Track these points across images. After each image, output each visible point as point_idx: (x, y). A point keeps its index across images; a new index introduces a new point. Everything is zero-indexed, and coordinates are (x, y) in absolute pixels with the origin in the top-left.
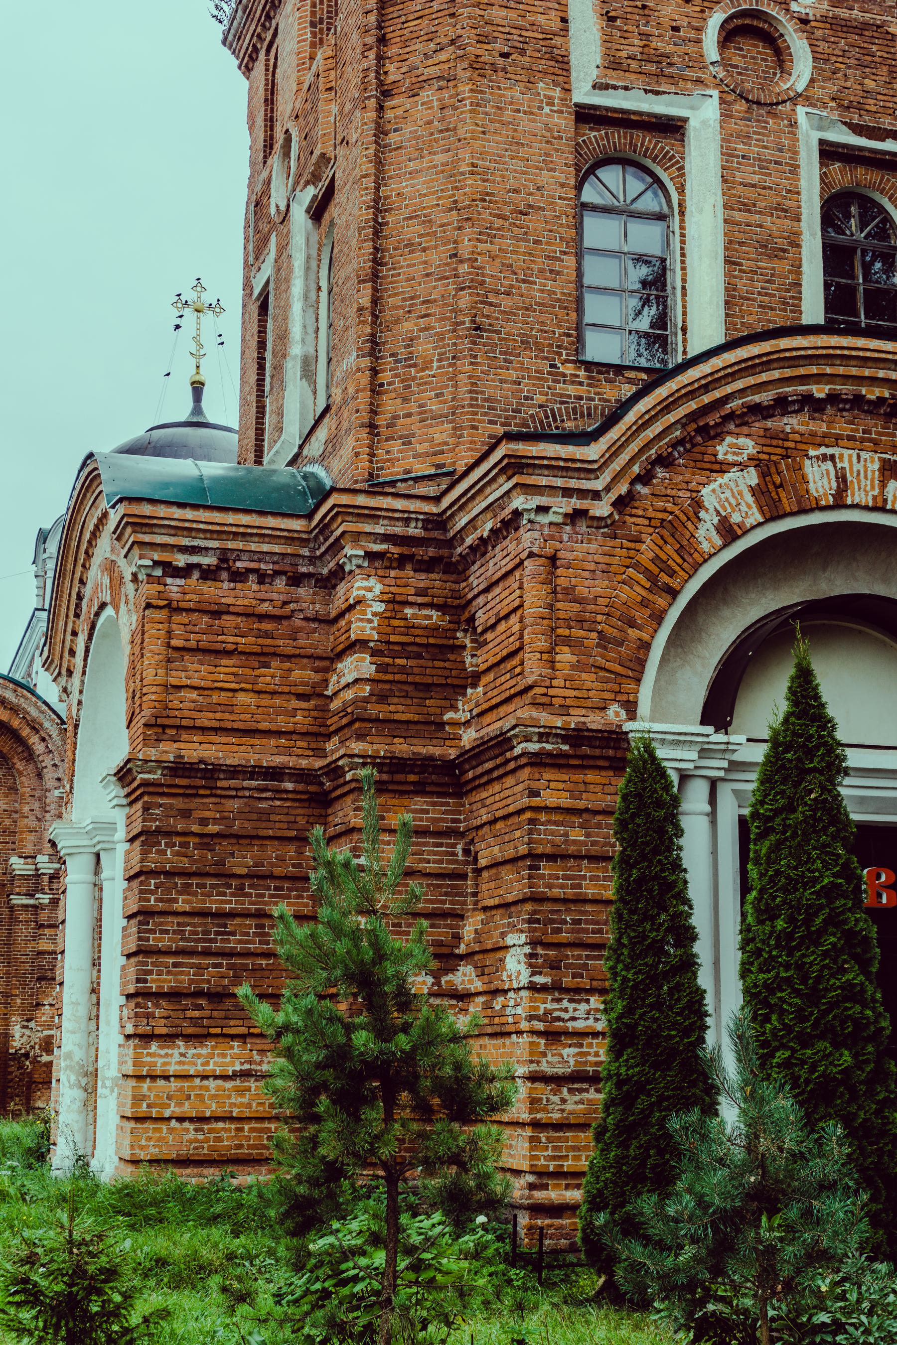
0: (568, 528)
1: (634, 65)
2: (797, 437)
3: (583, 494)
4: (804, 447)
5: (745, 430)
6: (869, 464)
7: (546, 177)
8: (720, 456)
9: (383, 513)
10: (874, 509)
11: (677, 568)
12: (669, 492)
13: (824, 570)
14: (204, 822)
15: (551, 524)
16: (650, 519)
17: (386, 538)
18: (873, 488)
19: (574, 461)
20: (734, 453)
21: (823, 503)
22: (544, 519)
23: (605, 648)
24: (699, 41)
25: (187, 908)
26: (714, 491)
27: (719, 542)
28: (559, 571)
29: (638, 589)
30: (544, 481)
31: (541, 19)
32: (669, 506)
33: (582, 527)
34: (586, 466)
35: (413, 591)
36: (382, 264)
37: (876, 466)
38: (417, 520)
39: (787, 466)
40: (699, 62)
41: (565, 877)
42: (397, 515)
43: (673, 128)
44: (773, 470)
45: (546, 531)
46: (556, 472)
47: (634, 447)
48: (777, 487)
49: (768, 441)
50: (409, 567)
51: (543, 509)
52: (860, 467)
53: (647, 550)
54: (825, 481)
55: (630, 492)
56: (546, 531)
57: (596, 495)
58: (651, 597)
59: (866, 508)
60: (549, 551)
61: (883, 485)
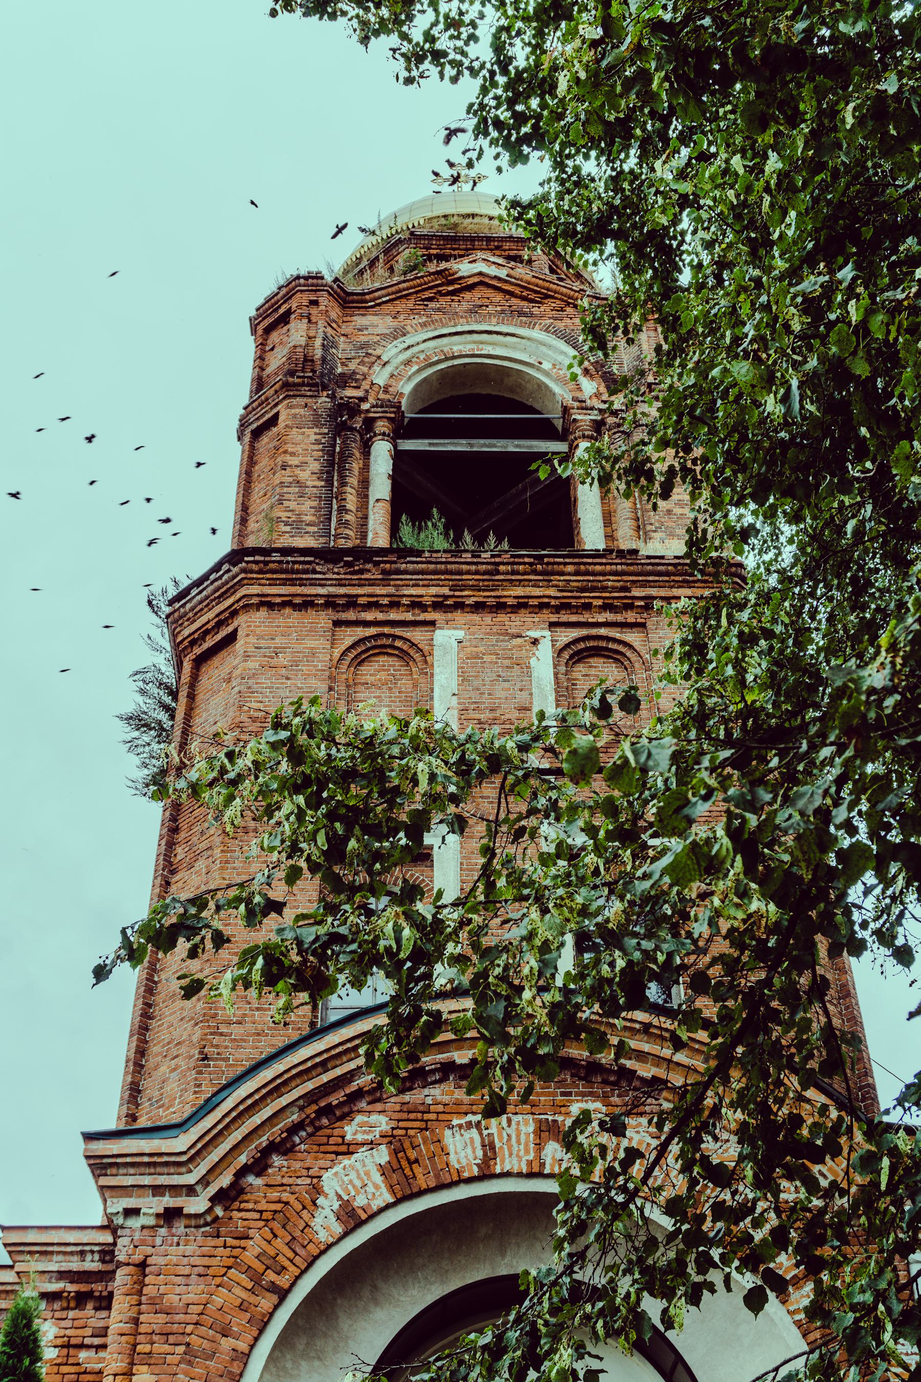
0: (163, 1231)
2: (440, 1108)
3: (175, 1190)
4: (447, 1117)
5: (379, 1106)
6: (522, 1127)
8: (349, 1137)
9: (56, 1248)
10: (531, 1175)
11: (287, 1263)
12: (285, 1181)
13: (503, 1255)
15: (143, 1227)
16: (261, 1212)
17: (62, 1275)
18: (527, 1152)
19: (160, 1155)
20: (365, 1132)
21: (466, 1175)
22: (135, 1223)
23: (190, 1363)
26: (336, 1174)
27: (338, 1229)
28: (147, 1280)
29: (237, 1291)
30: (129, 1181)
32: (285, 1196)
33: (180, 1227)
34: (173, 1159)
35: (89, 1331)
36: (151, 1018)
37: (531, 1128)
38: (92, 1252)
39: (425, 1140)
42: (69, 1249)
44: (407, 1144)
45: (137, 1236)
46: (142, 1170)
47: (237, 1136)
48: (411, 1163)
49: (405, 1116)
50: (90, 1306)
51: (130, 1212)
54: (469, 1150)
55: (233, 1185)
56: (137, 1236)
57: (190, 1190)
58: (253, 1299)
59: (520, 1175)
60: (138, 1258)
61: (539, 1147)
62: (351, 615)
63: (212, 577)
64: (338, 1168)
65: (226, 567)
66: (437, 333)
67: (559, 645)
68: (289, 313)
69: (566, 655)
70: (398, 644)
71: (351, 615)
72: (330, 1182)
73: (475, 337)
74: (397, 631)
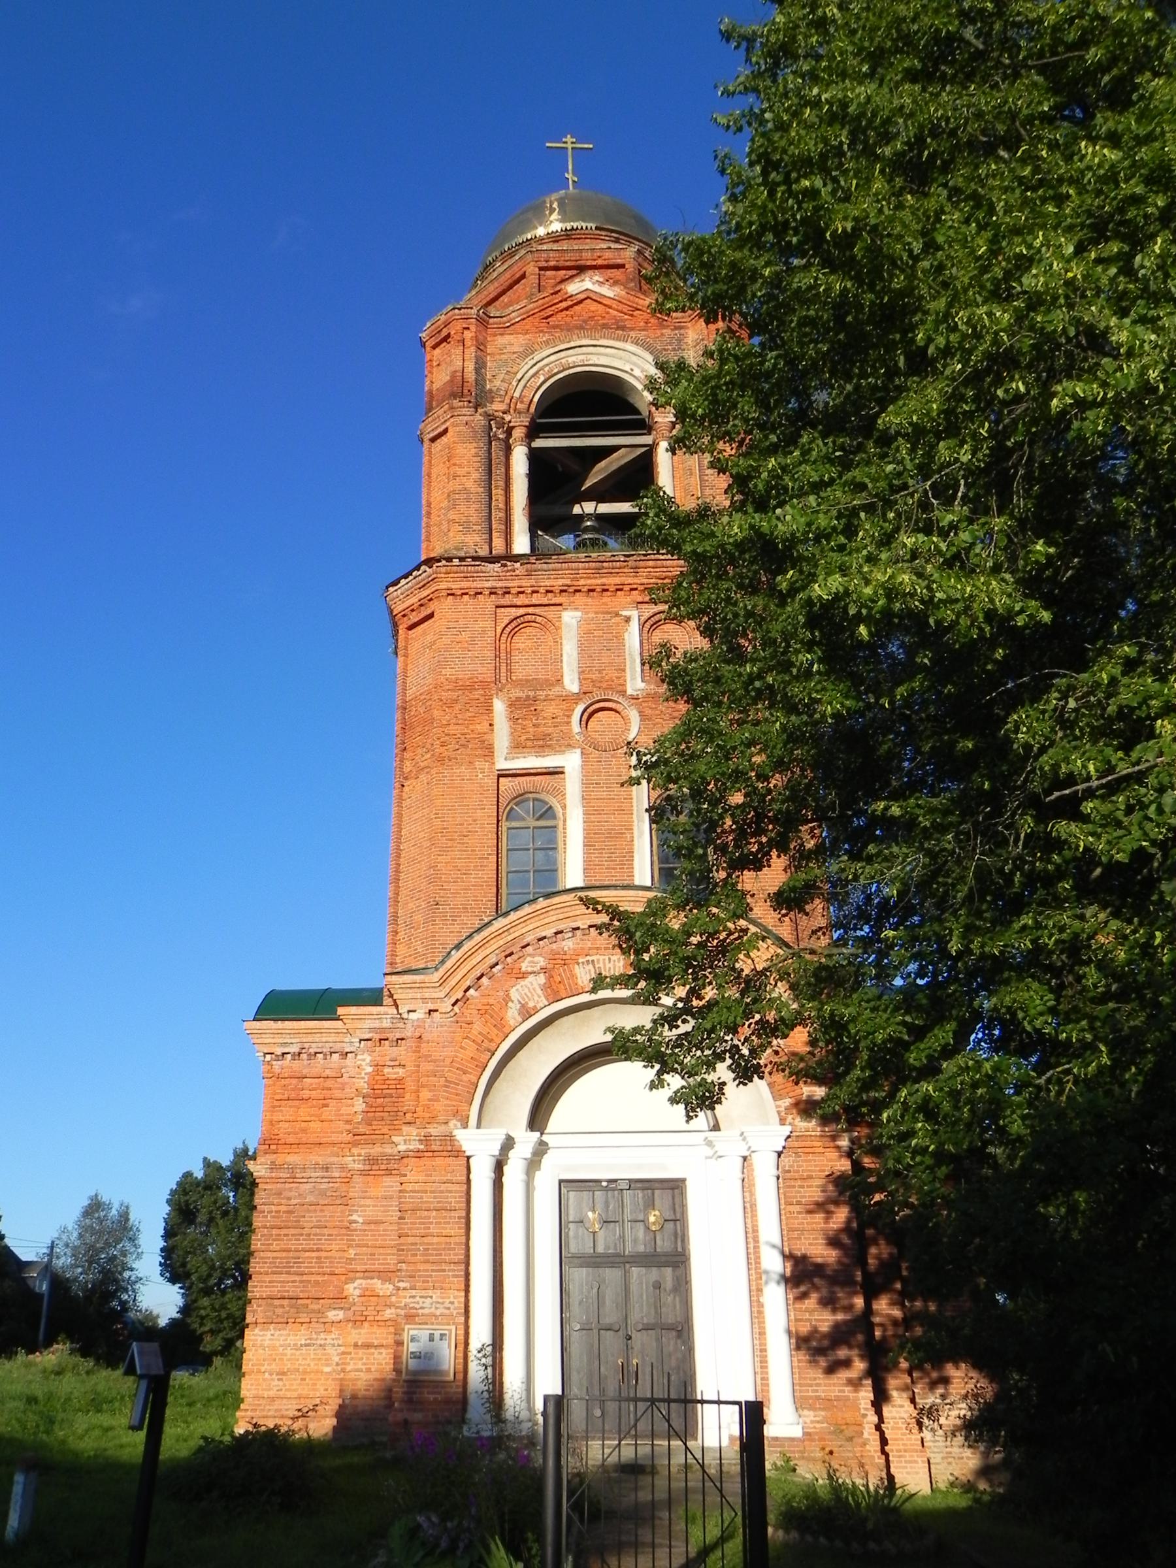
1: (529, 743)
7: (479, 813)
8: (523, 969)
14: (289, 1199)
24: (569, 723)
25: (278, 1248)
31: (478, 727)
35: (388, 1058)
40: (568, 735)
41: (421, 1223)
43: (557, 772)
52: (611, 965)
53: (477, 1027)
60: (418, 1034)
62: (507, 600)
63: (415, 573)
64: (518, 987)
65: (423, 568)
66: (556, 349)
67: (643, 619)
68: (448, 336)
69: (648, 625)
70: (539, 619)
71: (507, 600)
72: (514, 994)
73: (584, 350)
74: (537, 610)
